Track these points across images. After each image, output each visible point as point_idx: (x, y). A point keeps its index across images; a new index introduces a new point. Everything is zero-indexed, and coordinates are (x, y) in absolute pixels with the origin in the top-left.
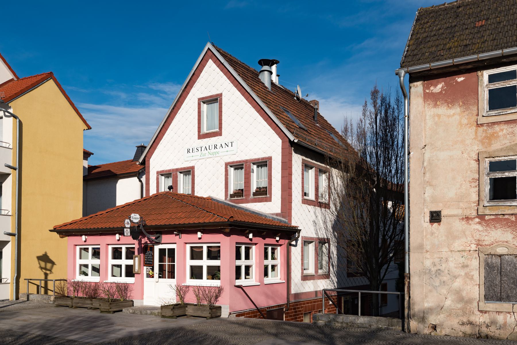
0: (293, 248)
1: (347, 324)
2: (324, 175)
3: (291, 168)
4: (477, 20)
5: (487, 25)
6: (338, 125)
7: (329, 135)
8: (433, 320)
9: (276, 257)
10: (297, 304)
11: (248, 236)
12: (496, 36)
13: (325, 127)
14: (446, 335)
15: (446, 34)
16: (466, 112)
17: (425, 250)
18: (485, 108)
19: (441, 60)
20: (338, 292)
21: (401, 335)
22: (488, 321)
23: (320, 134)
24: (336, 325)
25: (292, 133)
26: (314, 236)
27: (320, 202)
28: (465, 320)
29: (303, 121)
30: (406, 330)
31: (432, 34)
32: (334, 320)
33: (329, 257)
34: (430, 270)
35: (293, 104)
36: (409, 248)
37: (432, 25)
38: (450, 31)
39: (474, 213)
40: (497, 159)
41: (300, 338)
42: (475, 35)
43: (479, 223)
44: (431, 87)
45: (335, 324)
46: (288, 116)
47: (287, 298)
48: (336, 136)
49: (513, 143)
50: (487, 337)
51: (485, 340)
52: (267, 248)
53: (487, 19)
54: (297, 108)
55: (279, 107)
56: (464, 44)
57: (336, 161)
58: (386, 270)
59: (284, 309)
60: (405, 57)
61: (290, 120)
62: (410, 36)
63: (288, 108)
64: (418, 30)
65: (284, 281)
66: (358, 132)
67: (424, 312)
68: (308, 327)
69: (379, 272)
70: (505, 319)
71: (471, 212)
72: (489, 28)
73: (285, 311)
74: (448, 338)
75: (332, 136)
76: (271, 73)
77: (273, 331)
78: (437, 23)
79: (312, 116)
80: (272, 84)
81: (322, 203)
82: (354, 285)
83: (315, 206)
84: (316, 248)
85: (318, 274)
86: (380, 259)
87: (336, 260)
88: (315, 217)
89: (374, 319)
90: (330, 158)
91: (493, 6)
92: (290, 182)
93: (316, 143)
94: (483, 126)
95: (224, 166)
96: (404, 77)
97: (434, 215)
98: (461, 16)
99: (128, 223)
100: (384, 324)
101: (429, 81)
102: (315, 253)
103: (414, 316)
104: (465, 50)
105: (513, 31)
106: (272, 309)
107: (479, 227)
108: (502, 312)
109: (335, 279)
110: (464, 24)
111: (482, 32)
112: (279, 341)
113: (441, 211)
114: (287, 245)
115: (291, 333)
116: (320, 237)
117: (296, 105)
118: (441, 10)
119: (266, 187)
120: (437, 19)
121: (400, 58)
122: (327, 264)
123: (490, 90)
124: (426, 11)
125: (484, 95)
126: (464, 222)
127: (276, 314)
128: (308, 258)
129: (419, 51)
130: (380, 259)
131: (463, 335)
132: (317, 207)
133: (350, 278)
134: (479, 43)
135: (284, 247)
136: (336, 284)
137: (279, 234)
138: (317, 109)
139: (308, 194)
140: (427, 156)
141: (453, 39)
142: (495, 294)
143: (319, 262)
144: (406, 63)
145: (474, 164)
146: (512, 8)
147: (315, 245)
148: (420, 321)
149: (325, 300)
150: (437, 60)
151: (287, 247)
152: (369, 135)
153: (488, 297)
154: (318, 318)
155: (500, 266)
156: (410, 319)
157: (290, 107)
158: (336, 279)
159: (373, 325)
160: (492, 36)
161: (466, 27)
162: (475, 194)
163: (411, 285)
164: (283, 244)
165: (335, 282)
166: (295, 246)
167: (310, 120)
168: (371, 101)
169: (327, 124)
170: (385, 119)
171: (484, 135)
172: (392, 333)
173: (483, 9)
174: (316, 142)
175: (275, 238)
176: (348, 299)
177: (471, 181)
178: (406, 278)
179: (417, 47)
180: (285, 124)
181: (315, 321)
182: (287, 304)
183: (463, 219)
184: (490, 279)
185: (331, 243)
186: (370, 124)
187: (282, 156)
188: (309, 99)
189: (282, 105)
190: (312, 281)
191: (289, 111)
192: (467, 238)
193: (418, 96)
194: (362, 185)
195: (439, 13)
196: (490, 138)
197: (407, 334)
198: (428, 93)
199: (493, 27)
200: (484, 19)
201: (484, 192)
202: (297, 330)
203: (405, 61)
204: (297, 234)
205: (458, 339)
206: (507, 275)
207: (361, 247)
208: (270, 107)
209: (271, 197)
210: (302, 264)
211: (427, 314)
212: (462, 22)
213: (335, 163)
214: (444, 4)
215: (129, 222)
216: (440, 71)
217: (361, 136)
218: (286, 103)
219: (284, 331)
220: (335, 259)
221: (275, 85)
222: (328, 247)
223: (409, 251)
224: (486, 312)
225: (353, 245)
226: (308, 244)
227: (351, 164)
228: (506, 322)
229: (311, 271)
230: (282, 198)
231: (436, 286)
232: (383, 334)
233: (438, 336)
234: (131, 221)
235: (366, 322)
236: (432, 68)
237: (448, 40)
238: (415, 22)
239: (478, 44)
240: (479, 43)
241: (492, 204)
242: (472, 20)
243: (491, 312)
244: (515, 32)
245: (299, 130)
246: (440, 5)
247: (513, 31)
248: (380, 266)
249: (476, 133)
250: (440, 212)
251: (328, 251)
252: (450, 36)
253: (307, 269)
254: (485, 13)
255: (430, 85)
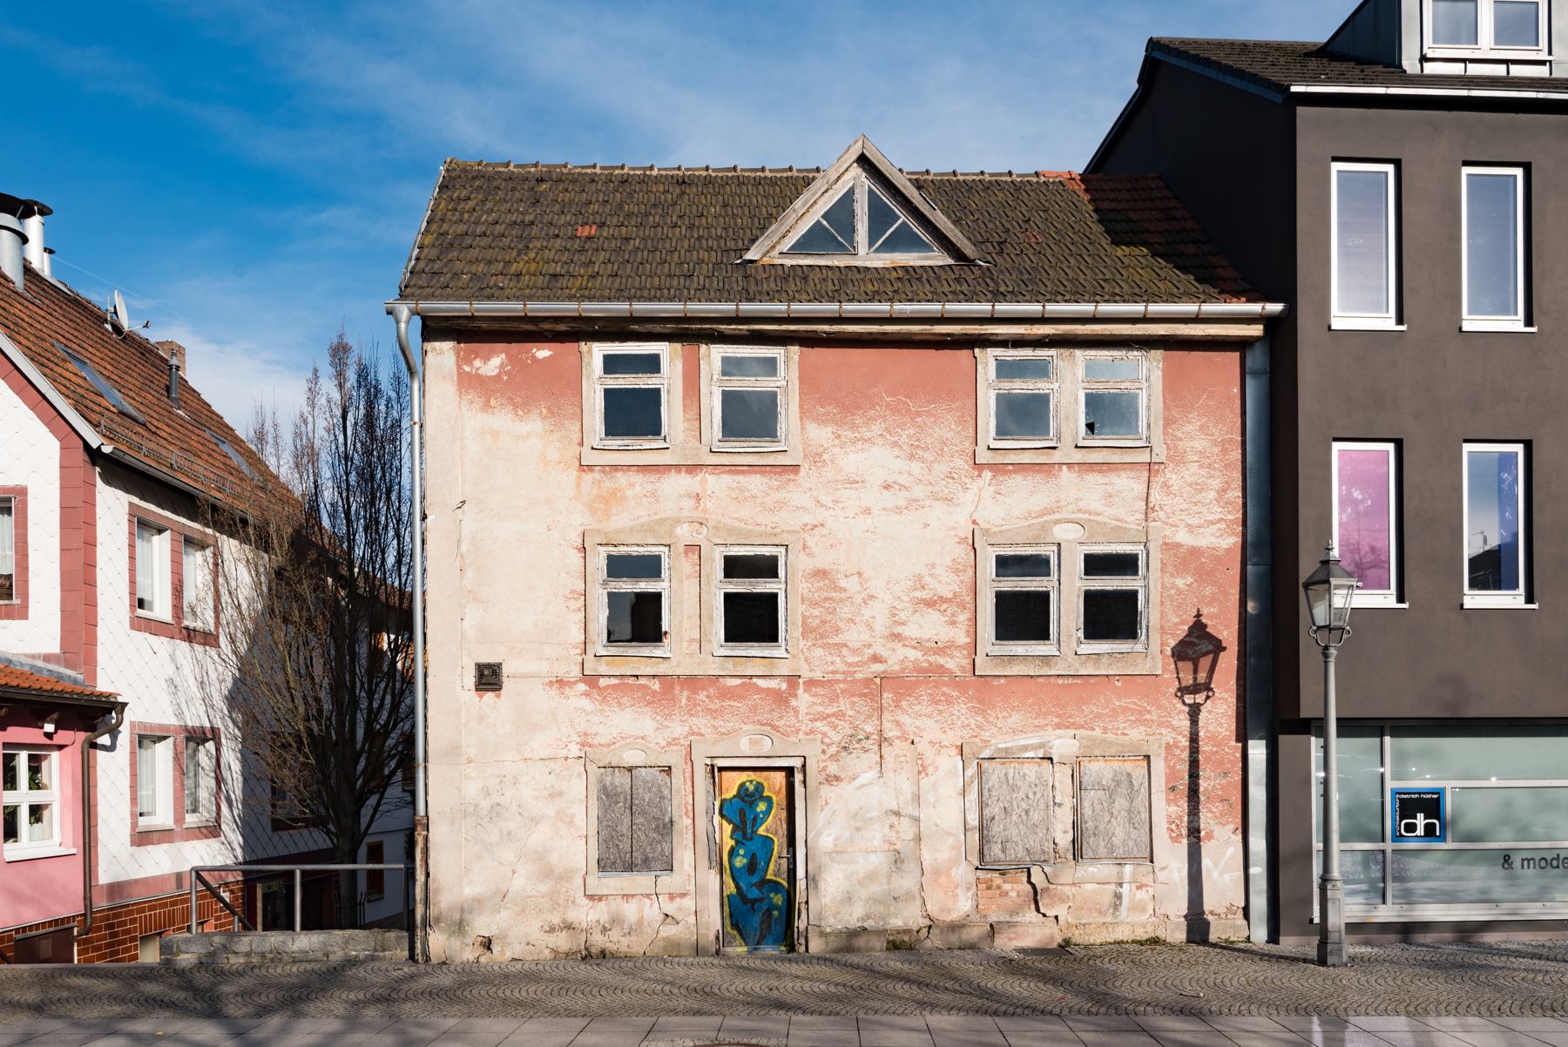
0: (101, 755)
1: (263, 955)
2: (199, 554)
3: (91, 524)
4: (580, 222)
5: (601, 239)
6: (241, 422)
7: (217, 445)
8: (483, 926)
9: (45, 780)
10: (115, 912)
12: (618, 268)
13: (204, 422)
14: (514, 960)
15: (509, 238)
16: (555, 434)
17: (464, 758)
18: (597, 430)
19: (498, 299)
20: (245, 873)
21: (406, 970)
22: (604, 918)
23: (187, 439)
24: (231, 962)
25: (96, 426)
26: (171, 720)
27: (187, 628)
28: (556, 920)
29: (131, 394)
30: (420, 958)
31: (479, 230)
32: (225, 948)
33: (219, 780)
34: (477, 806)
35: (99, 341)
36: (426, 752)
37: (478, 208)
38: (519, 233)
39: (576, 672)
40: (622, 550)
41: (117, 1009)
42: (574, 255)
43: (587, 694)
44: (475, 359)
45: (228, 958)
46: (84, 374)
47: (85, 898)
48: (237, 451)
49: (654, 518)
50: (603, 954)
51: (598, 962)
52: (14, 755)
53: (602, 225)
54: (112, 355)
55: (53, 345)
56: (551, 271)
57: (232, 519)
58: (376, 810)
59: (75, 930)
60: (411, 273)
61: (87, 386)
62: (425, 224)
63: (81, 350)
64: (444, 211)
65: (73, 851)
66: (296, 447)
67: (462, 910)
68: (148, 973)
69: (357, 814)
70: (641, 910)
71: (568, 669)
72: (605, 246)
73: (80, 934)
74: (519, 966)
75: (226, 448)
76: (24, 240)
77: (31, 996)
78: (489, 205)
79: (163, 386)
80: (28, 270)
81: (194, 630)
82: (293, 850)
83: (172, 638)
84: (176, 754)
85: (185, 826)
86: (361, 781)
87: (240, 786)
88: (174, 668)
89: (338, 935)
90: (214, 508)
91: (614, 197)
92: (90, 565)
93: (173, 462)
94: (593, 470)
96: (408, 322)
97: (486, 672)
98: (545, 203)
100: (364, 947)
101: (470, 345)
102: (175, 770)
103: (438, 920)
104: (552, 285)
105: (654, 265)
106: (34, 933)
107: (585, 703)
108: (633, 896)
109: (236, 839)
110: (551, 224)
111: (590, 253)
112: (46, 1025)
113: (501, 664)
114: (82, 747)
115: (90, 997)
116: (190, 724)
117: (109, 347)
118: (500, 178)
119: (10, 577)
120: (490, 198)
121: (399, 273)
122: (213, 799)
123: (606, 391)
124: (464, 170)
125: (594, 400)
126: (554, 692)
127: (46, 947)
128: (153, 782)
129: (446, 265)
130: (361, 781)
131: (553, 955)
132: (178, 642)
133: (281, 833)
134: (582, 276)
135: (73, 754)
136: (239, 852)
137: (55, 716)
138: (178, 368)
139: (151, 603)
140: (468, 527)
141: (527, 255)
142: (620, 857)
143: (186, 792)
144: (413, 290)
145: (577, 558)
146: (653, 212)
147: (175, 745)
148: (454, 932)
149: (197, 897)
150: (490, 297)
151: (82, 753)
152: (325, 458)
153: (605, 863)
154: (178, 947)
155: (629, 792)
156: (428, 929)
157: (91, 349)
158: (240, 839)
159: (335, 952)
160: (610, 265)
161: (556, 232)
162: (578, 626)
163: (431, 845)
164: (70, 743)
165: (236, 845)
166: (111, 748)
167: (157, 395)
168: (332, 371)
169: (209, 414)
170: (370, 421)
171: (595, 492)
172: (384, 967)
173: (594, 200)
174: (174, 458)
175: (42, 728)
176: (275, 888)
178: (419, 828)
179: (441, 253)
180: (71, 395)
181: (169, 957)
182: (84, 915)
183: (551, 683)
184: (610, 823)
185: (223, 740)
186: (328, 431)
187: (62, 488)
188: (153, 336)
189: (62, 339)
190: (165, 846)
191: (87, 361)
193: (444, 378)
194: (305, 588)
195: (495, 184)
196: (610, 500)
197: (422, 967)
198: (467, 373)
199: (613, 245)
200: (594, 223)
201: (596, 622)
202: (110, 986)
203: (412, 283)
204: (114, 714)
205: (540, 967)
206: (644, 813)
207: (307, 750)
208: (20, 339)
209: (27, 607)
210: (134, 800)
211: (470, 913)
212: (546, 218)
213: (233, 525)
214: (507, 165)
216: (496, 326)
217: (306, 456)
218: (76, 337)
219: (65, 994)
220: (235, 783)
221: (42, 280)
222: (214, 752)
223: (426, 760)
224: (600, 898)
225: (283, 746)
226: (152, 744)
227: (278, 530)
228: (642, 918)
229: (163, 816)
230: (62, 611)
231: (491, 845)
232: (360, 972)
233: (495, 963)
235: (316, 946)
236: (476, 314)
237: (514, 254)
238: (437, 190)
239: (580, 278)
240: (582, 276)
241: (613, 651)
242: (568, 218)
243: (612, 897)
244: (657, 268)
245: (117, 419)
246: (498, 165)
247: (654, 265)
248: (360, 802)
249: (578, 485)
250: (499, 665)
251: (214, 761)
252: (520, 246)
253: (149, 814)
254: (596, 209)
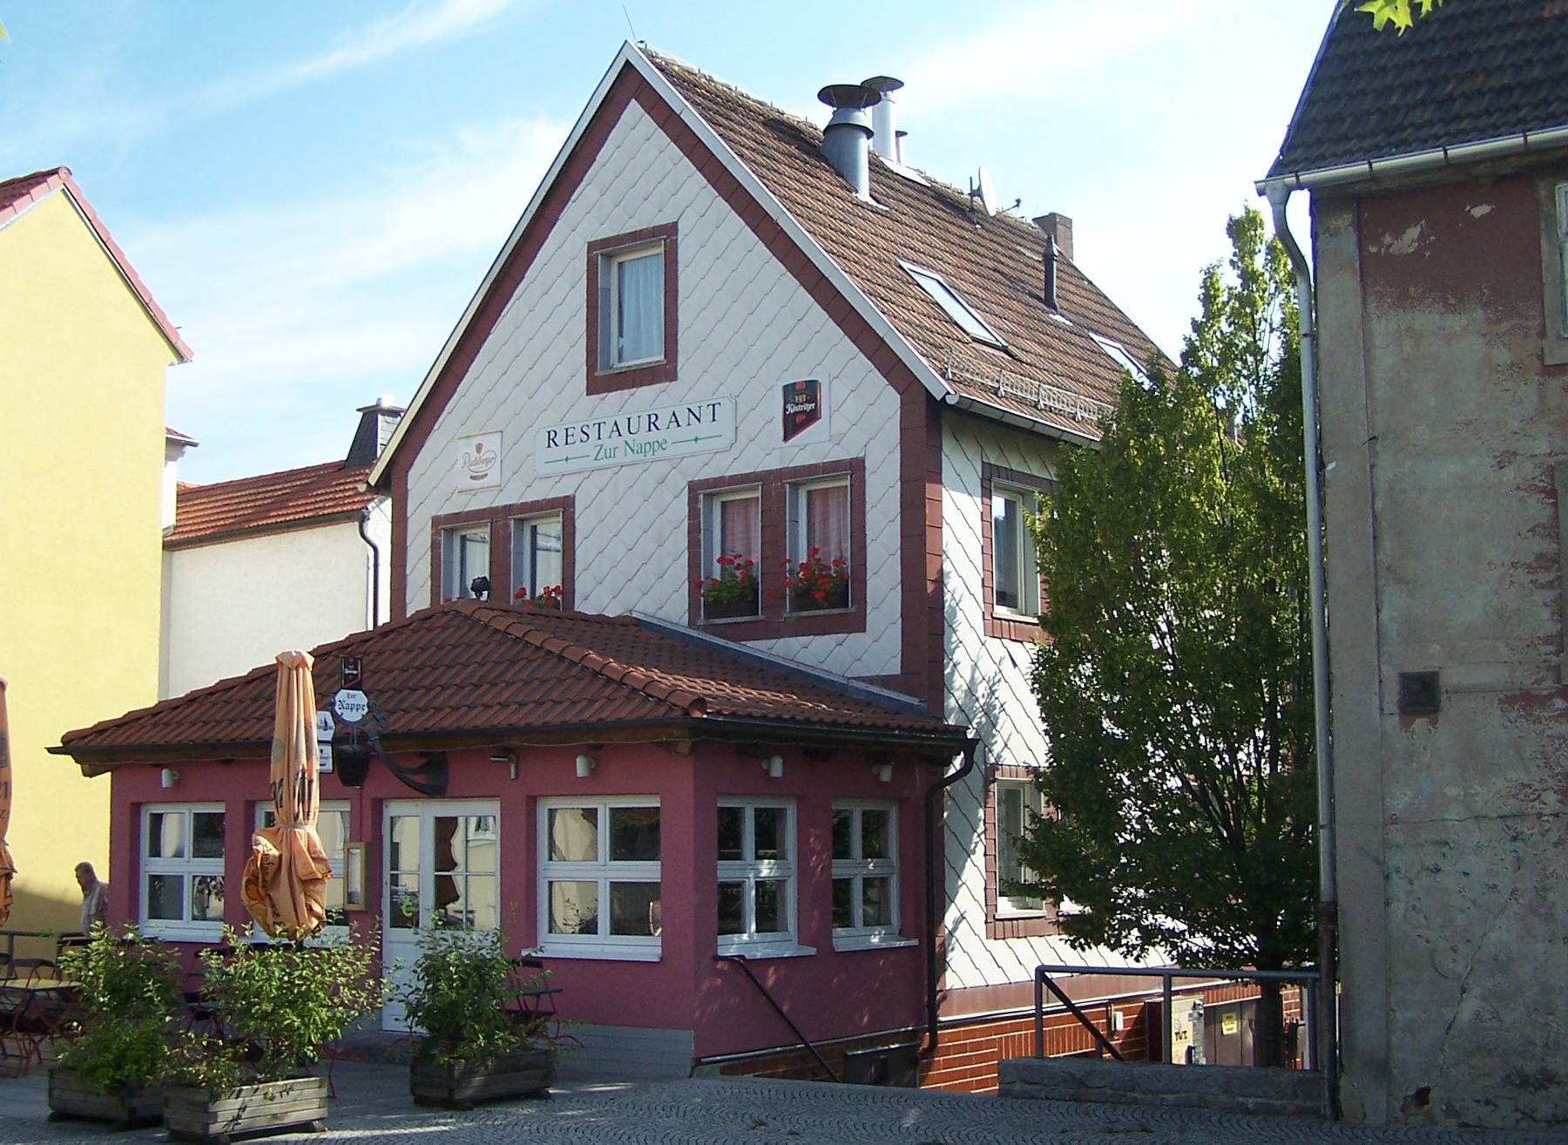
11: (764, 766)
44: (1383, 234)
95: (682, 507)
99: (326, 723)
177: (1534, 565)
183: (1510, 701)
192: (1527, 771)
215: (331, 723)
234: (334, 714)
255: (1380, 231)
